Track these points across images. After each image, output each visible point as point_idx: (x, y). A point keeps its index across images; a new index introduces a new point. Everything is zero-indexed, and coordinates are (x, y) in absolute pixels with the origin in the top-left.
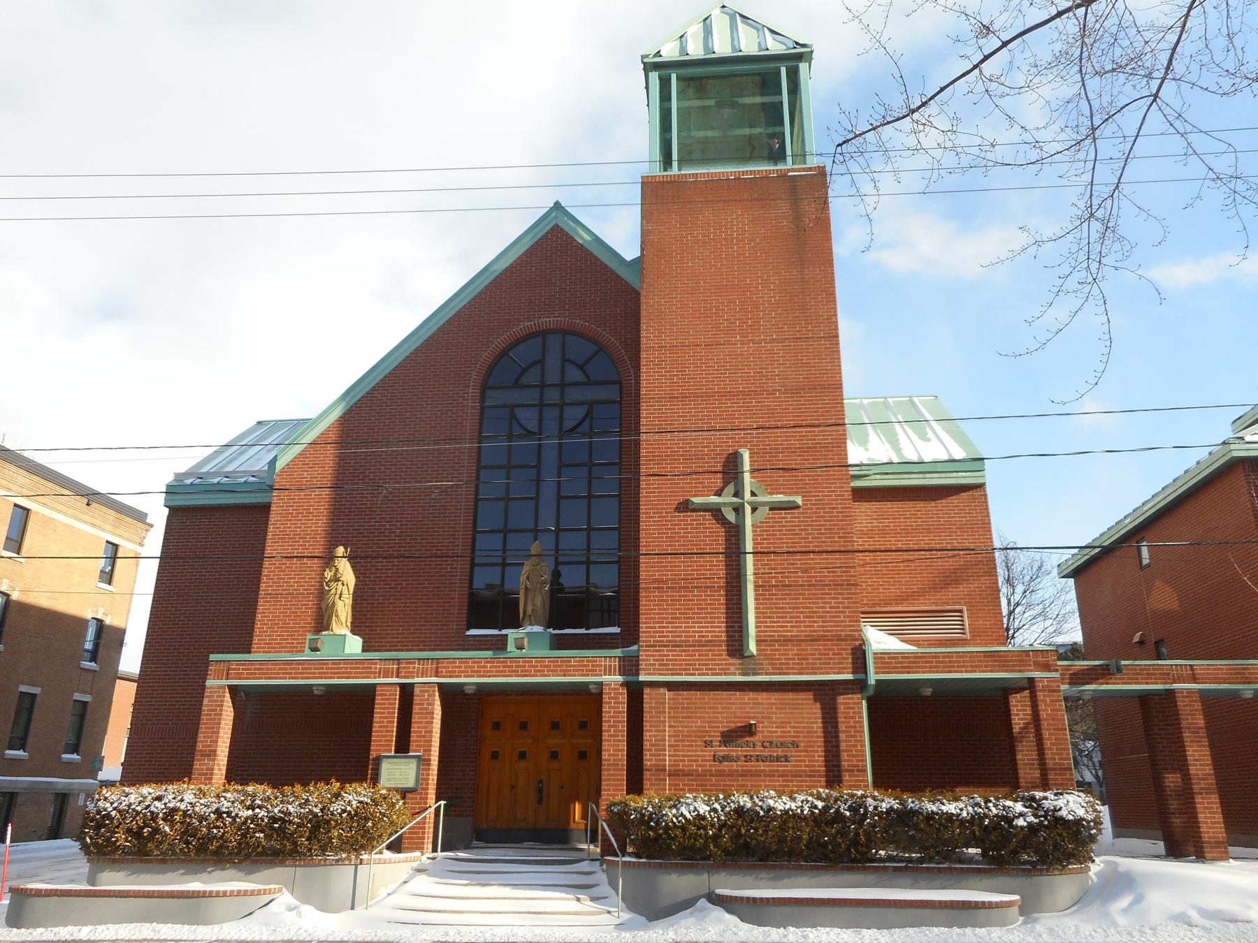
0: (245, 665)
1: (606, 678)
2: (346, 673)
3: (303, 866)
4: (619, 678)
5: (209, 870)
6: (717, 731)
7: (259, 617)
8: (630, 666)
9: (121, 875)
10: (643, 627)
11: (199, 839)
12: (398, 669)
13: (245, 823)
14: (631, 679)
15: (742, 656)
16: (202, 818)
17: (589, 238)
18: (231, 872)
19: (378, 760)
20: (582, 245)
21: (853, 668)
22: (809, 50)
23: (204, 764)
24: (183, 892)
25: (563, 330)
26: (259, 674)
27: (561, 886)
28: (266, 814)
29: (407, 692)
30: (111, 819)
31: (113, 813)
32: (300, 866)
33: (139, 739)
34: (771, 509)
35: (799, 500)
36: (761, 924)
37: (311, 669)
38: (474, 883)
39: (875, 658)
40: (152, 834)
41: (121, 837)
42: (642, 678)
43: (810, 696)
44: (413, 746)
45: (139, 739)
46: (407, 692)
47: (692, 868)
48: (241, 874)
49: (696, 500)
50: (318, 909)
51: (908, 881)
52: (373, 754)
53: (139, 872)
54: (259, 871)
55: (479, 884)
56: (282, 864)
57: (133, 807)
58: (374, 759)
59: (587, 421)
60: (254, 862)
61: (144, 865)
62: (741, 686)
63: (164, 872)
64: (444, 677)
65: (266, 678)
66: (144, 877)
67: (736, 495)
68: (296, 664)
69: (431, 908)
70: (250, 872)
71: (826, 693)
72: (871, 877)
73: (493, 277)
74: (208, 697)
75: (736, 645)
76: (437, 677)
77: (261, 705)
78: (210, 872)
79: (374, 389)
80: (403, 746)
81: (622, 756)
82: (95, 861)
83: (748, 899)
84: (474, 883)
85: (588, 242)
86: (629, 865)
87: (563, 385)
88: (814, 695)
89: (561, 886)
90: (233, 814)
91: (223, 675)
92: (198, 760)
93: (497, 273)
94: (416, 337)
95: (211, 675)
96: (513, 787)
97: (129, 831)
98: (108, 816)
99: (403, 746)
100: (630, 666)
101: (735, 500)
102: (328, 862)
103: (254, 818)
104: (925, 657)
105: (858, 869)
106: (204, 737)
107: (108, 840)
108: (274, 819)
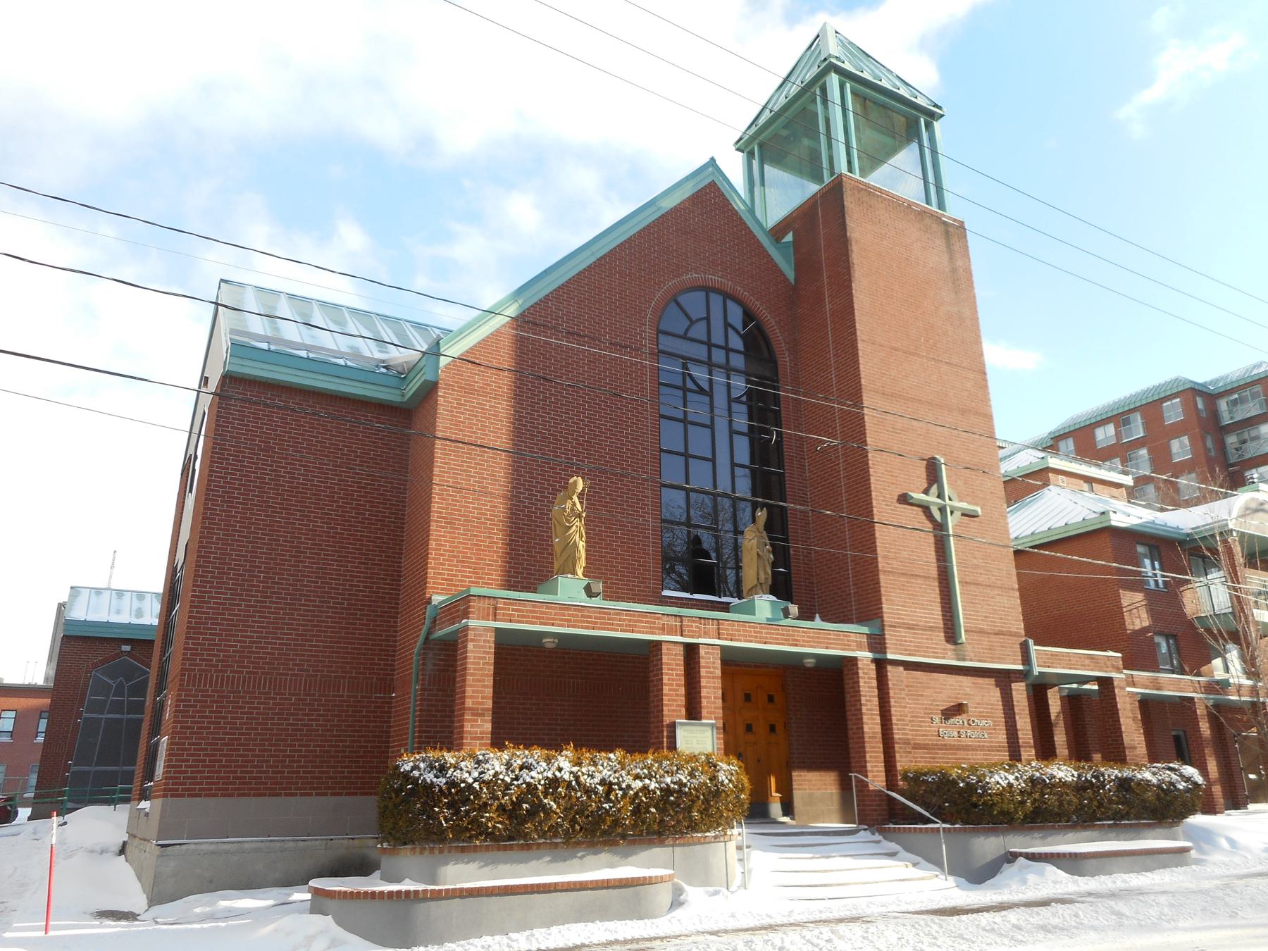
0: (515, 604)
1: (858, 654)
2: (630, 626)
3: (684, 845)
4: (870, 655)
5: (580, 854)
6: (937, 710)
7: (433, 544)
8: (877, 643)
9: (472, 867)
10: (885, 607)
11: (588, 816)
12: (681, 626)
13: (636, 794)
14: (879, 656)
15: (955, 643)
16: (588, 791)
17: (742, 207)
18: (604, 857)
19: (673, 726)
20: (736, 212)
21: (1022, 660)
22: (942, 113)
23: (478, 726)
24: (581, 883)
25: (726, 293)
26: (533, 617)
27: (881, 854)
28: (657, 785)
29: (691, 652)
30: (477, 795)
31: (476, 785)
32: (679, 845)
33: (437, 690)
34: (963, 515)
35: (979, 510)
36: (1081, 874)
37: (591, 617)
38: (818, 856)
39: (1037, 654)
40: (532, 813)
41: (491, 819)
42: (890, 656)
43: (992, 681)
44: (704, 713)
45: (437, 690)
46: (691, 652)
47: (994, 831)
48: (616, 859)
49: (915, 495)
50: (969, 882)
51: (1114, 834)
52: (667, 720)
53: (495, 862)
54: (636, 854)
55: (823, 857)
56: (661, 843)
57: (501, 777)
58: (668, 726)
59: (696, 388)
60: (633, 842)
61: (501, 854)
62: (990, 672)
63: (526, 861)
64: (726, 639)
65: (542, 624)
66: (503, 868)
67: (939, 496)
68: (575, 610)
69: (870, 881)
70: (627, 856)
71: (1004, 679)
72: (1095, 834)
73: (660, 214)
74: (472, 640)
75: (951, 635)
76: (719, 638)
77: (444, 655)
78: (581, 858)
79: (547, 298)
80: (693, 712)
81: (878, 729)
82: (436, 852)
83: (1070, 854)
84: (818, 856)
85: (742, 210)
86: (918, 830)
87: (710, 345)
88: (996, 681)
89: (881, 854)
90: (624, 786)
91: (488, 615)
92: (469, 721)
93: (663, 212)
94: (588, 253)
95: (473, 612)
96: (759, 761)
97: (502, 809)
98: (470, 786)
99: (693, 712)
100: (877, 643)
101: (939, 501)
102: (707, 840)
103: (645, 788)
104: (1057, 655)
105: (1089, 826)
106: (473, 692)
107: (474, 821)
108: (667, 791)
